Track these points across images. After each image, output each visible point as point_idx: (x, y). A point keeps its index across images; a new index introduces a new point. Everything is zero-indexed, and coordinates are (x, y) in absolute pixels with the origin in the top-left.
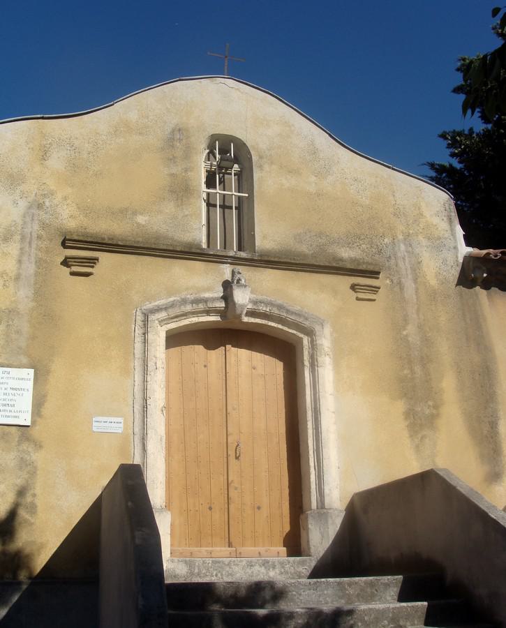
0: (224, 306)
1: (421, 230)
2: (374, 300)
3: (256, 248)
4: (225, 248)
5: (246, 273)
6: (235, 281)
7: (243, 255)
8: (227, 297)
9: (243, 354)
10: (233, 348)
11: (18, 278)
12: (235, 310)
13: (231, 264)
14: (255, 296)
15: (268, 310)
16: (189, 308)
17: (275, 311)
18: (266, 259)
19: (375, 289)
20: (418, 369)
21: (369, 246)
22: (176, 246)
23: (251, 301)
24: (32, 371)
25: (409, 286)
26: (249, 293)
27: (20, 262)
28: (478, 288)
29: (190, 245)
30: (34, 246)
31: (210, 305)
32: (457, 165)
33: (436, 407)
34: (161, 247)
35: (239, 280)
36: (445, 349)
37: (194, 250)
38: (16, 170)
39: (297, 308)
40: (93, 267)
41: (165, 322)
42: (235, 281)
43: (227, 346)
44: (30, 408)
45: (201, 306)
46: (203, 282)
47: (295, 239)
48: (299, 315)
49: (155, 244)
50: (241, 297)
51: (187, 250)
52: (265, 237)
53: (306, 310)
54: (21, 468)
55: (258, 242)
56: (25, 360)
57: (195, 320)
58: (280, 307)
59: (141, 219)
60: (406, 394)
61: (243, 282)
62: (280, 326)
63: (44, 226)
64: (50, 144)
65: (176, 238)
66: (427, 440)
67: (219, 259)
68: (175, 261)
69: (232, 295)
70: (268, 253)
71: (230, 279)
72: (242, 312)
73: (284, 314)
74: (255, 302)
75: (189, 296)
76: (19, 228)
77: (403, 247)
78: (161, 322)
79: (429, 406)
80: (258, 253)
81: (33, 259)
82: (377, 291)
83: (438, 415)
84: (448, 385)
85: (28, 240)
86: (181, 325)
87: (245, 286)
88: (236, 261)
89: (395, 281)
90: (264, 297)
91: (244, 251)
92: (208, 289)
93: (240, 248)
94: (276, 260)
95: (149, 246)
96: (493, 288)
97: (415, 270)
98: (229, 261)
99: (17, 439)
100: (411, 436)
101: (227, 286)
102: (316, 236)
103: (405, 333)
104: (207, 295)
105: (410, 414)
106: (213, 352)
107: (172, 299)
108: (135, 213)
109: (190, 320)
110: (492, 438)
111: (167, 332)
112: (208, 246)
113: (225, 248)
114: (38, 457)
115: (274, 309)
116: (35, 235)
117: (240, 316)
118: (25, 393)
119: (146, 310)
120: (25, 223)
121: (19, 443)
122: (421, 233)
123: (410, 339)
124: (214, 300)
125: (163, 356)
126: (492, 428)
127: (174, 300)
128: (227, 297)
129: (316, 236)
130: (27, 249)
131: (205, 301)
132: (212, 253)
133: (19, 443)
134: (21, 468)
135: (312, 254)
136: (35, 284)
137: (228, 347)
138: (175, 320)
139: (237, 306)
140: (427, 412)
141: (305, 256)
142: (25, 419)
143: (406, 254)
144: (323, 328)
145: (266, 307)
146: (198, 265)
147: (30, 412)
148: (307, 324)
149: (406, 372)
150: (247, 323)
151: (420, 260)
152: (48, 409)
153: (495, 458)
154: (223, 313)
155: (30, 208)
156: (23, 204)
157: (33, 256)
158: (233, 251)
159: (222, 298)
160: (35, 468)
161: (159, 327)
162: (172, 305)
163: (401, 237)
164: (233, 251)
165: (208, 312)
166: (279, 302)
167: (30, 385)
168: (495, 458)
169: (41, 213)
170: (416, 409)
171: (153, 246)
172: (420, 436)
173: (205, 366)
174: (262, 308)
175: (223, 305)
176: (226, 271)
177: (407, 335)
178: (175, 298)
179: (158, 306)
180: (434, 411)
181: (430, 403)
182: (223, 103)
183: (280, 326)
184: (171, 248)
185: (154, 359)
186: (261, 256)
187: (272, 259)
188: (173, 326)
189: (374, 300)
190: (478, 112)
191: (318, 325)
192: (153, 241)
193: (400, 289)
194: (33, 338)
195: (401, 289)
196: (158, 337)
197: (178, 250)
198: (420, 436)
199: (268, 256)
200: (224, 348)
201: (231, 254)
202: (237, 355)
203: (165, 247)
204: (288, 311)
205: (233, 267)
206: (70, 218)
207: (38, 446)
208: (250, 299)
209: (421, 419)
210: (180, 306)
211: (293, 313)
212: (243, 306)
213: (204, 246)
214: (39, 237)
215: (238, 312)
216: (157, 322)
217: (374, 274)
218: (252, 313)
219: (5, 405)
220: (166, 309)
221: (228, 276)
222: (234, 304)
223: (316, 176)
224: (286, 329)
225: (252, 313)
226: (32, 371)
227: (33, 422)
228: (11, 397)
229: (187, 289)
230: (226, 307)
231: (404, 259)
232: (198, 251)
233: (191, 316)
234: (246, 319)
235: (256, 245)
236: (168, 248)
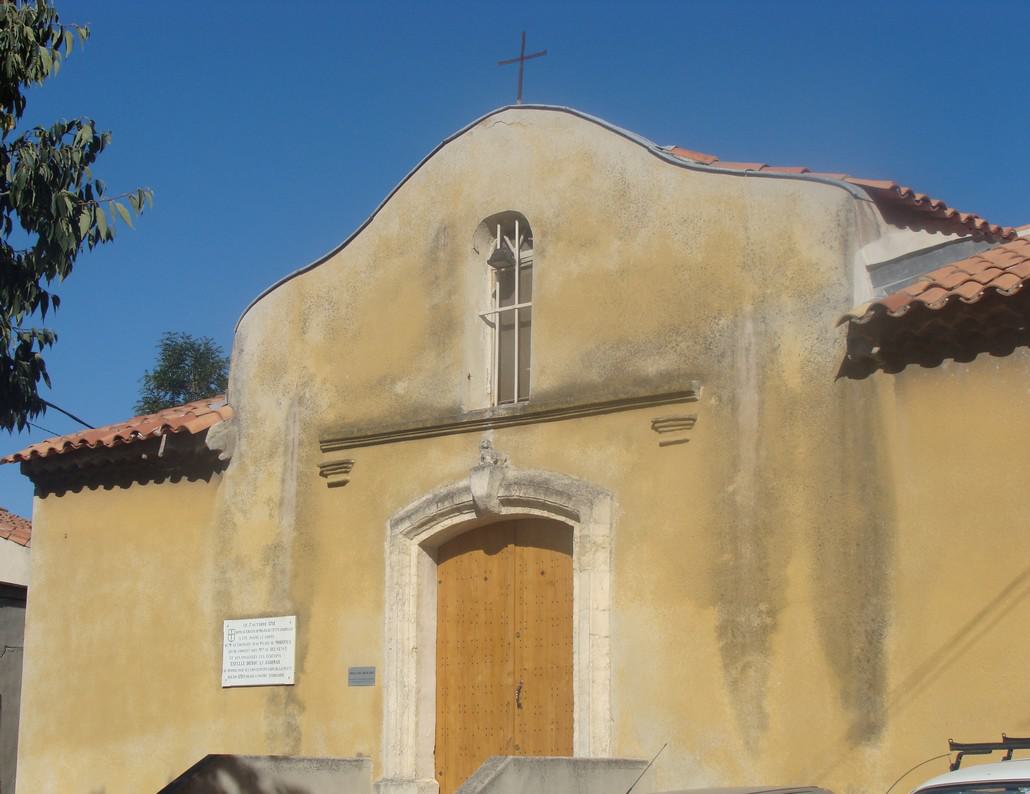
1: (788, 283)
2: (687, 441)
11: (281, 503)
16: (433, 510)
19: (689, 422)
20: (747, 550)
21: (690, 343)
24: (293, 618)
25: (749, 397)
27: (283, 481)
28: (880, 372)
30: (296, 456)
33: (772, 613)
36: (798, 505)
40: (347, 472)
44: (292, 664)
45: (447, 505)
51: (438, 424)
54: (288, 735)
56: (289, 605)
57: (448, 523)
59: (400, 388)
60: (722, 595)
63: (306, 426)
64: (309, 308)
65: (435, 404)
66: (751, 672)
76: (283, 436)
77: (749, 327)
79: (761, 612)
81: (294, 477)
82: (692, 425)
83: (774, 627)
84: (798, 573)
85: (291, 449)
86: (454, 523)
89: (725, 398)
94: (544, 409)
96: (909, 367)
97: (763, 367)
99: (284, 701)
100: (726, 666)
103: (731, 489)
105: (727, 629)
108: (393, 382)
109: (442, 524)
110: (868, 661)
114: (301, 720)
116: (297, 443)
118: (288, 646)
120: (288, 427)
121: (287, 704)
122: (787, 288)
123: (738, 498)
126: (870, 643)
129: (612, 347)
130: (289, 463)
133: (287, 704)
134: (288, 735)
136: (297, 507)
138: (425, 528)
140: (756, 622)
142: (289, 678)
143: (753, 340)
144: (592, 509)
146: (456, 440)
147: (293, 668)
149: (726, 557)
151: (776, 344)
152: (309, 665)
153: (869, 698)
155: (291, 406)
156: (285, 402)
157: (295, 469)
160: (300, 733)
162: (416, 511)
163: (748, 308)
167: (291, 635)
168: (869, 698)
169: (303, 409)
170: (738, 619)
172: (739, 665)
173: (486, 579)
177: (734, 493)
180: (769, 621)
181: (763, 607)
182: (524, 153)
184: (420, 426)
188: (424, 536)
189: (687, 441)
190: (32, 417)
191: (585, 504)
193: (732, 409)
194: (295, 576)
195: (735, 410)
197: (429, 425)
198: (739, 665)
206: (329, 409)
207: (302, 708)
209: (744, 636)
214: (301, 444)
217: (684, 396)
219: (272, 662)
220: (409, 517)
223: (621, 238)
226: (293, 618)
227: (297, 679)
228: (277, 652)
231: (747, 350)
233: (442, 519)
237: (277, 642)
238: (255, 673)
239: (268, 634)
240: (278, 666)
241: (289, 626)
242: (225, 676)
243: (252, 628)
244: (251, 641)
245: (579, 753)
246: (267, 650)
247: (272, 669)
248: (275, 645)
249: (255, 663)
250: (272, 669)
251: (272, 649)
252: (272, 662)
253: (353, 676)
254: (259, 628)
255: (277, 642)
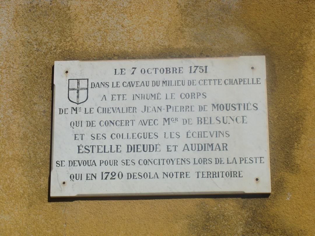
118: (250, 114)
142: (257, 178)
219: (203, 148)
227: (278, 183)
228: (217, 127)
237: (217, 106)
238: (151, 169)
239: (187, 89)
240: (222, 155)
241: (248, 74)
242: (59, 175)
243: (138, 77)
244: (140, 104)
245: (55, 61)
246: (186, 121)
247: (204, 161)
248: (211, 113)
249: (153, 148)
250: (204, 161)
251: (200, 121)
252: (203, 148)
253: (271, 155)
254: (160, 77)
255: (217, 106)
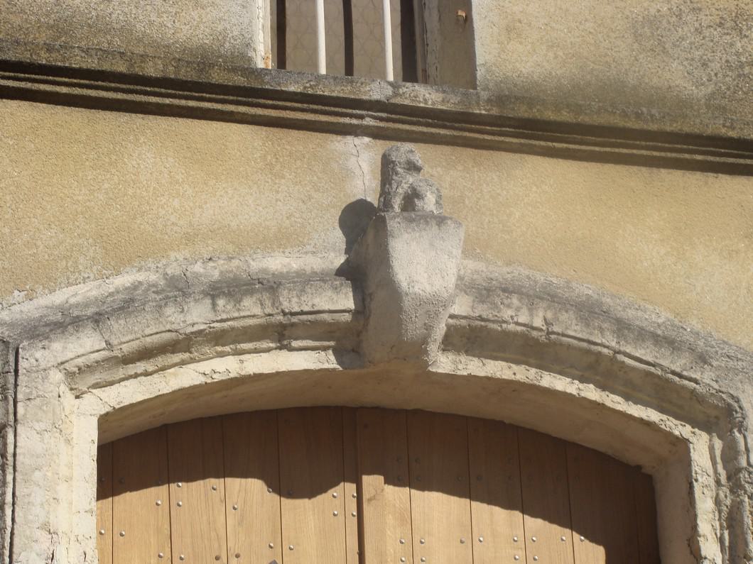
0: (349, 303)
3: (480, 73)
4: (349, 70)
5: (440, 172)
6: (397, 203)
7: (425, 95)
8: (364, 267)
9: (438, 511)
10: (390, 489)
12: (400, 323)
13: (376, 134)
14: (480, 266)
15: (538, 322)
16: (198, 315)
17: (571, 327)
18: (522, 112)
22: (143, 57)
23: (466, 286)
26: (457, 252)
29: (205, 59)
31: (291, 302)
32: (416, 200)
34: (77, 62)
35: (412, 198)
37: (217, 77)
38: (633, 179)
39: (656, 316)
41: (93, 379)
42: (397, 203)
43: (367, 480)
45: (252, 309)
46: (258, 208)
47: (637, 37)
48: (670, 343)
49: (50, 49)
50: (425, 266)
51: (186, 74)
52: (512, 30)
53: (694, 324)
55: (487, 49)
57: (225, 366)
58: (589, 311)
61: (429, 203)
62: (591, 392)
67: (322, 113)
68: (138, 120)
69: (384, 258)
70: (528, 94)
71: (373, 199)
72: (429, 328)
73: (607, 340)
74: (484, 291)
75: (198, 268)
78: (79, 377)
80: (486, 88)
87: (441, 220)
88: (397, 122)
90: (519, 272)
91: (426, 81)
92: (283, 240)
93: (410, 70)
95: (26, 57)
98: (368, 122)
101: (364, 225)
102: (721, 25)
104: (277, 263)
106: (303, 506)
107: (124, 280)
109: (206, 366)
111: (104, 421)
112: (281, 60)
113: (349, 70)
115: (564, 316)
117: (420, 348)
119: (12, 325)
124: (305, 280)
125: (88, 526)
127: (135, 286)
128: (364, 267)
131: (270, 285)
132: (292, 88)
135: (712, 96)
137: (372, 482)
138: (140, 367)
139: (407, 303)
141: (683, 105)
145: (532, 309)
146: (239, 141)
148: (706, 379)
150: (451, 380)
154: (347, 339)
158: (384, 79)
159: (341, 272)
161: (69, 397)
162: (127, 305)
164: (384, 79)
165: (281, 333)
166: (586, 289)
171: (43, 58)
174: (517, 316)
175: (346, 300)
176: (357, 164)
178: (141, 277)
179: (63, 309)
183: (591, 392)
184: (121, 68)
185: (43, 536)
186: (500, 99)
187: (550, 115)
188: (131, 392)
192: (43, 38)
196: (61, 442)
199: (531, 102)
200: (351, 488)
201: (377, 91)
202: (407, 519)
203: (92, 63)
204: (622, 327)
205: (381, 146)
208: (460, 278)
210: (159, 308)
211: (643, 335)
212: (433, 305)
213: (262, 54)
215: (413, 329)
216: (57, 376)
218: (469, 338)
220: (97, 320)
221: (365, 185)
222: (390, 285)
224: (615, 402)
225: (469, 338)
229: (189, 239)
230: (361, 311)
232: (240, 80)
234: (444, 363)
235: (480, 60)
236: (106, 67)
